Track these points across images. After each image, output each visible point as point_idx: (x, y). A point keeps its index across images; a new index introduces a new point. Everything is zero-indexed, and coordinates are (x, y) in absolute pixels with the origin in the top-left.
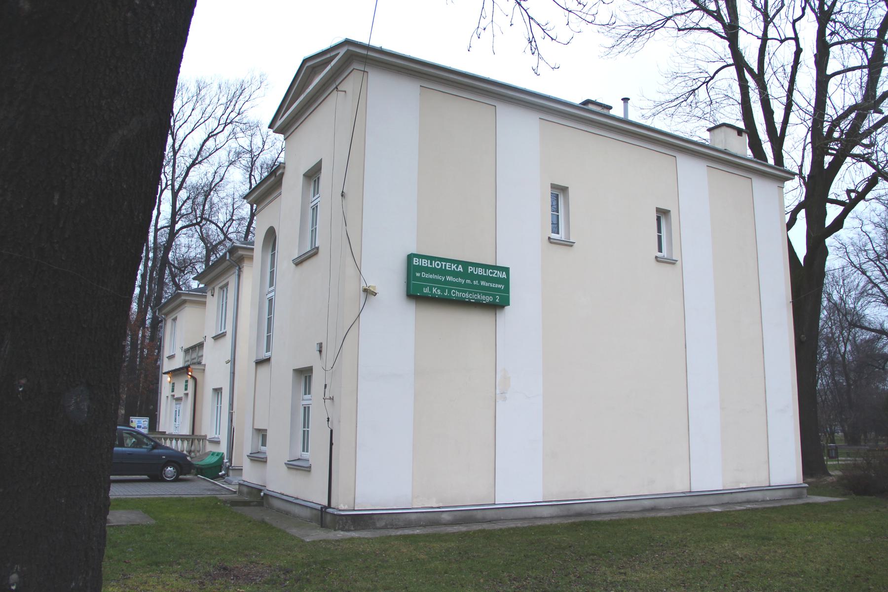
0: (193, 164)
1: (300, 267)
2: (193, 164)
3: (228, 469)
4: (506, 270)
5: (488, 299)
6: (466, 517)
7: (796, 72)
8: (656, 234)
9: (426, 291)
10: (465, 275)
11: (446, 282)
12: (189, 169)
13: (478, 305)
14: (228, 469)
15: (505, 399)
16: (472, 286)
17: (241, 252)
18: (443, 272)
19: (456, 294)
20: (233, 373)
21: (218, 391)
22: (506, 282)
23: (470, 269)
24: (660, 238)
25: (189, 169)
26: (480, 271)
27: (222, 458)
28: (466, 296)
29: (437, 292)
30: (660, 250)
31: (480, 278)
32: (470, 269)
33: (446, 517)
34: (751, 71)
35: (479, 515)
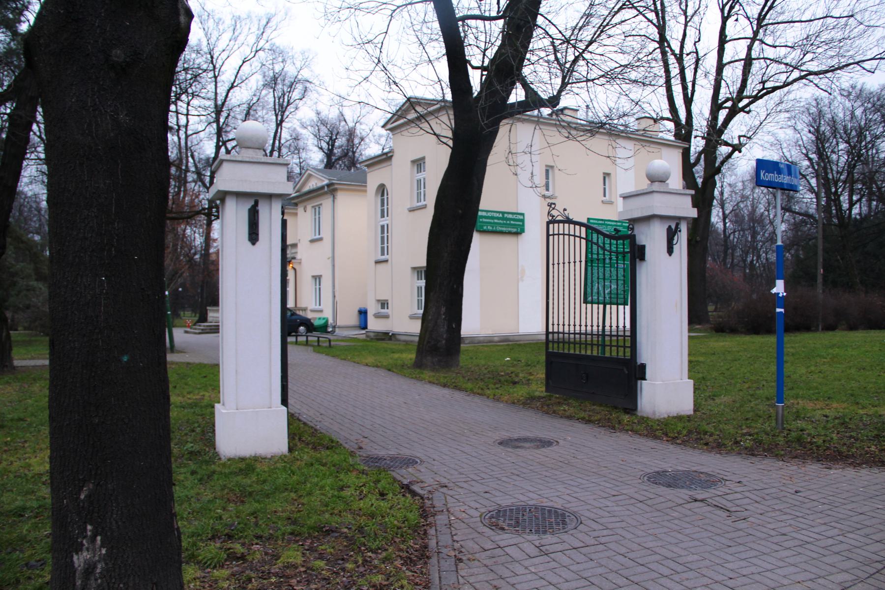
0: (232, 87)
1: (412, 213)
2: (232, 87)
3: (334, 327)
4: (523, 214)
5: (514, 230)
6: (505, 340)
7: (670, 106)
8: (602, 187)
9: (485, 228)
10: (503, 219)
11: (495, 223)
12: (228, 91)
13: (510, 233)
14: (334, 327)
15: (522, 281)
16: (506, 224)
17: (336, 186)
18: (493, 218)
19: (499, 229)
20: (334, 266)
21: (317, 278)
22: (523, 221)
23: (506, 215)
24: (605, 189)
25: (228, 91)
26: (510, 216)
27: (327, 321)
28: (504, 229)
29: (490, 228)
30: (605, 196)
31: (510, 219)
32: (506, 215)
33: (496, 339)
34: (673, 53)
35: (511, 338)
